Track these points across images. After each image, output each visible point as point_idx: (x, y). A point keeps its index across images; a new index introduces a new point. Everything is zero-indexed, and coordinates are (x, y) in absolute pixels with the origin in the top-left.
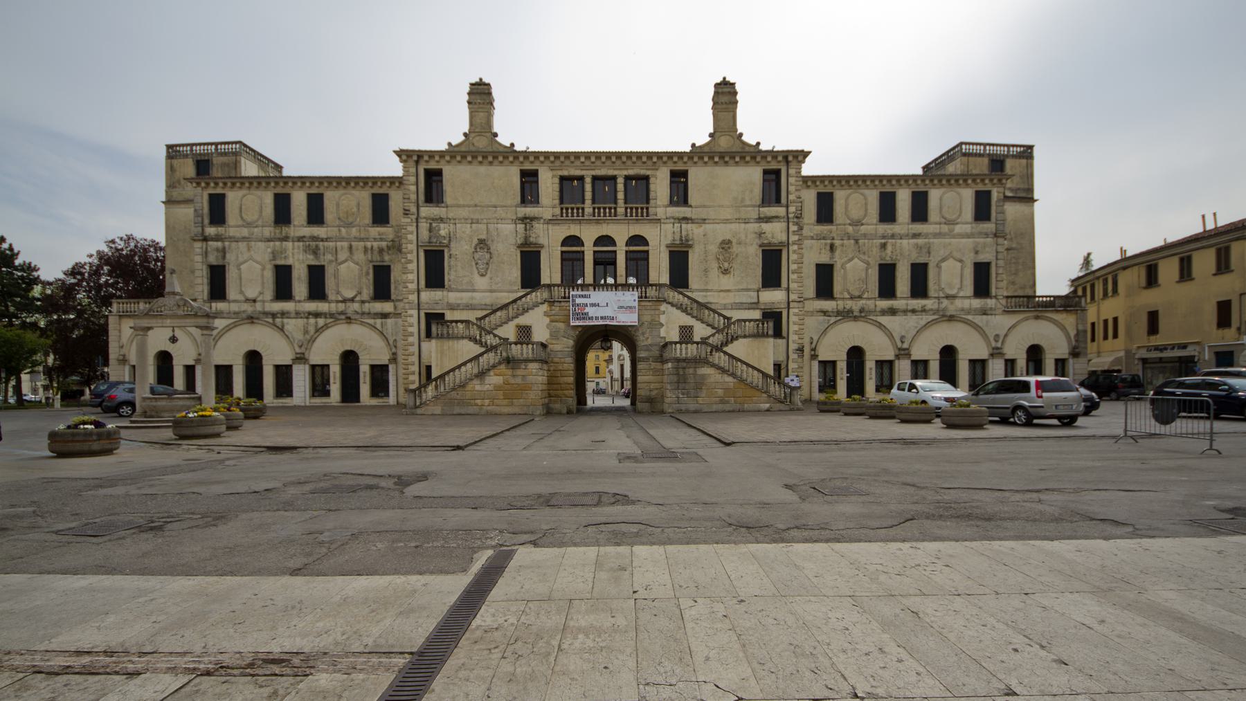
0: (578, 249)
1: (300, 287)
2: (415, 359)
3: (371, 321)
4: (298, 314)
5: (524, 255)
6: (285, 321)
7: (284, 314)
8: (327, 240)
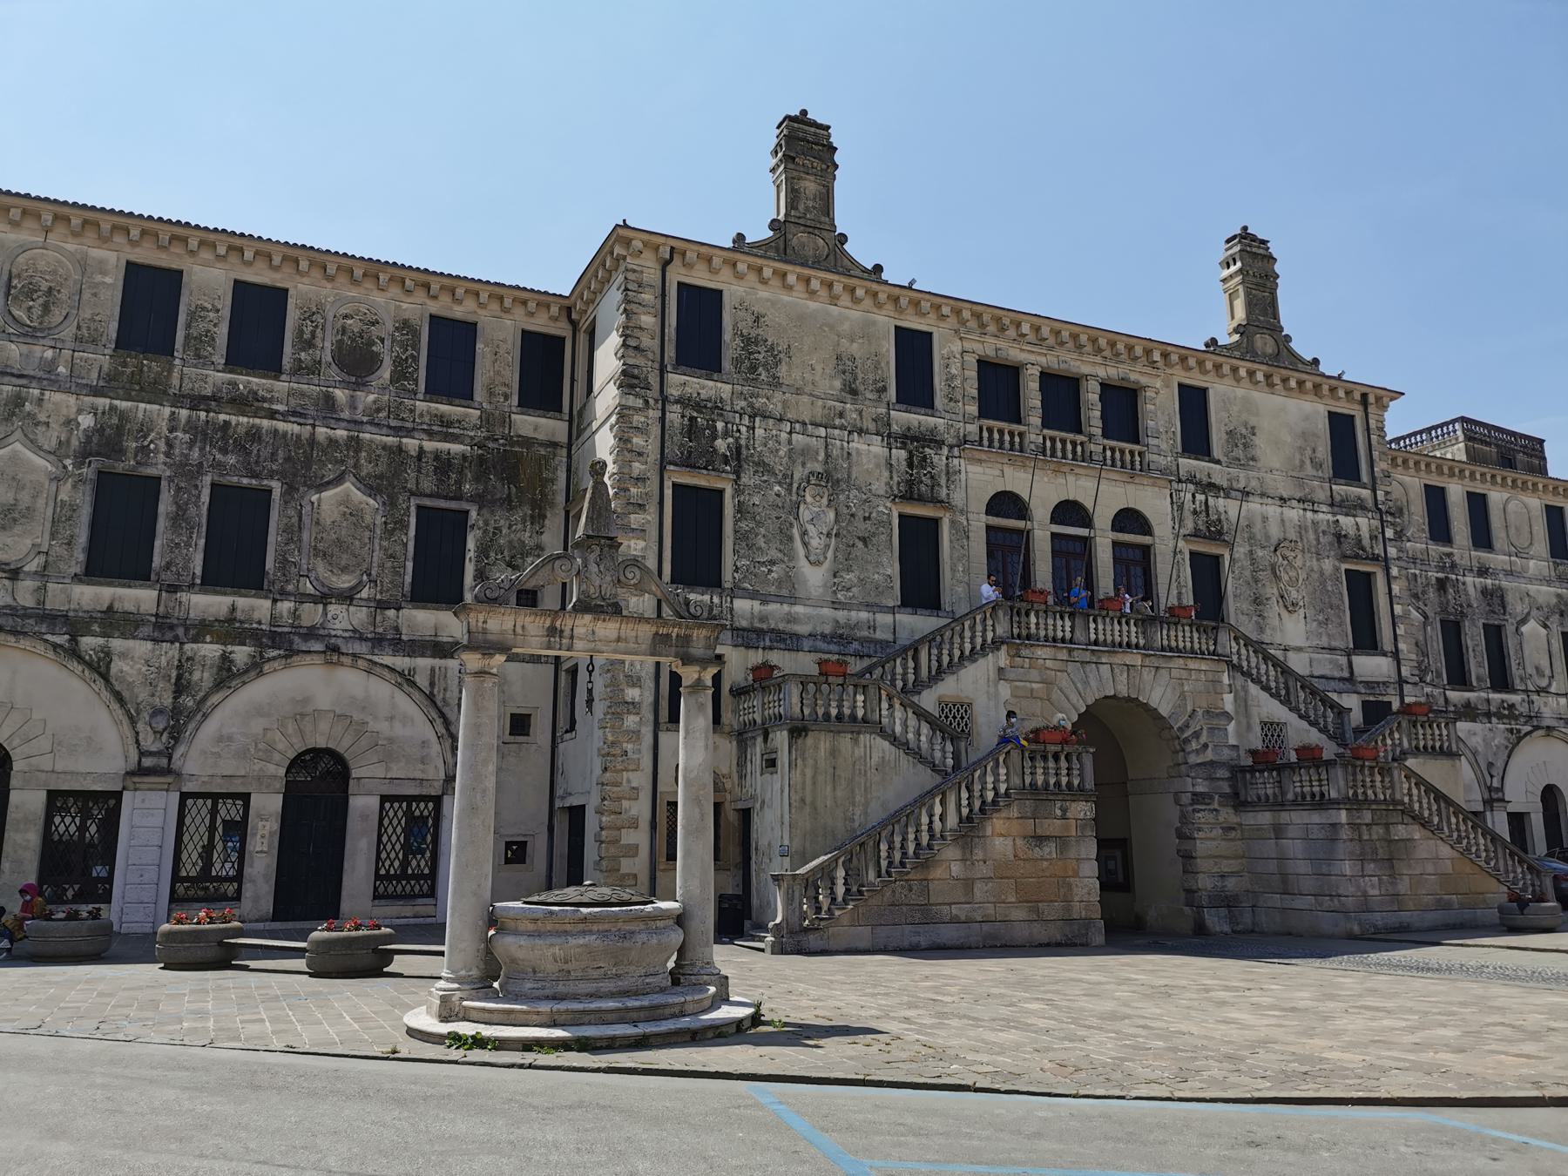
0: (1020, 524)
1: (178, 542)
2: (641, 779)
3: (401, 662)
4: (163, 627)
5: (106, 486)
6: (117, 644)
7: (115, 621)
8: (1227, 492)
